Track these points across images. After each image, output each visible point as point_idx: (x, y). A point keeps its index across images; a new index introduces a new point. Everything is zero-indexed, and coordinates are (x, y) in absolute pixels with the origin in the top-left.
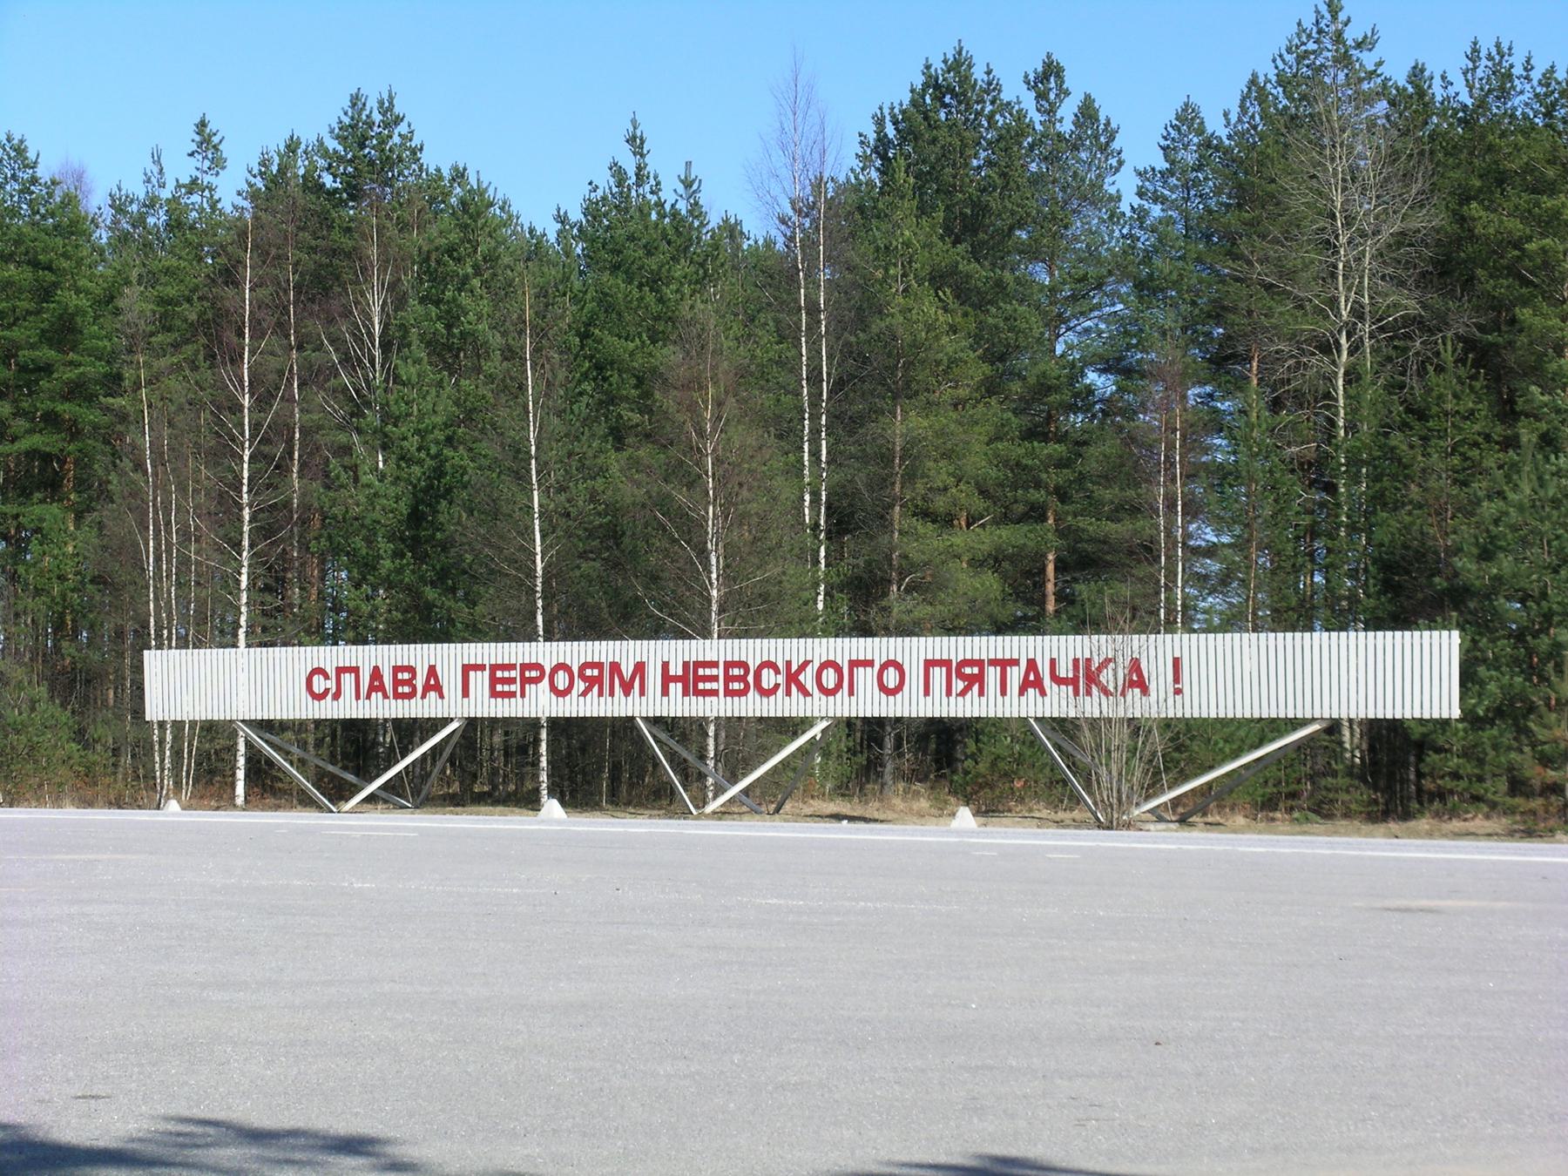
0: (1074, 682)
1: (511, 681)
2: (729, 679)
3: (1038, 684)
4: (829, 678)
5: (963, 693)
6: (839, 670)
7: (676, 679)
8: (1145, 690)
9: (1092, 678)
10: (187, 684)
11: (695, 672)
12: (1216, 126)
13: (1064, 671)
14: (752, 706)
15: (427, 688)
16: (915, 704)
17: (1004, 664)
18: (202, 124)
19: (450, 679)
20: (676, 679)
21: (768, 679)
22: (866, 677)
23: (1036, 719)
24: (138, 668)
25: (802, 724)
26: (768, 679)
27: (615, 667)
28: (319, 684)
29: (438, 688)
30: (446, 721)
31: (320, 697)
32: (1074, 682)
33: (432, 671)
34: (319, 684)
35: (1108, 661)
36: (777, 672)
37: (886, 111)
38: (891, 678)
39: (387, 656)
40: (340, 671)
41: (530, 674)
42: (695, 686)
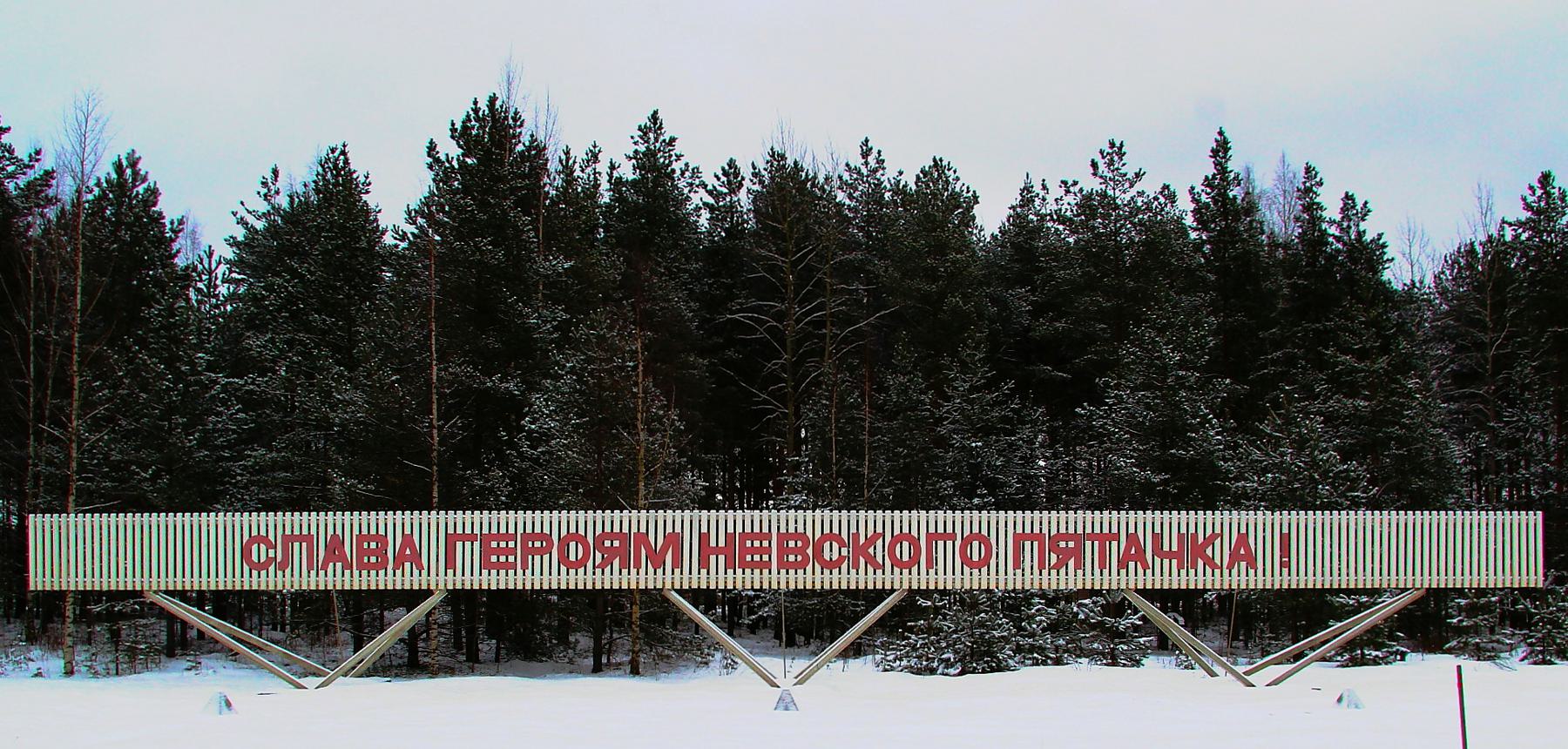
0: (1177, 555)
1: (508, 551)
2: (783, 551)
3: (1140, 556)
4: (905, 551)
5: (1057, 567)
6: (914, 543)
7: (717, 551)
8: (1252, 563)
9: (1198, 551)
10: (72, 549)
11: (742, 543)
12: (888, 176)
13: (1171, 543)
14: (813, 578)
15: (1235, 557)
16: (1002, 577)
17: (1105, 538)
18: (656, 112)
19: (434, 551)
20: (717, 551)
21: (831, 552)
22: (1220, 552)
23: (681, 592)
24: (1527, 505)
25: (878, 595)
26: (831, 552)
27: (642, 538)
28: (259, 553)
29: (416, 559)
30: (428, 593)
31: (260, 567)
32: (1177, 555)
33: (407, 540)
34: (259, 553)
35: (1214, 536)
36: (842, 544)
37: (242, 213)
38: (976, 550)
39: (349, 523)
40: (288, 540)
41: (535, 544)
42: (742, 558)
